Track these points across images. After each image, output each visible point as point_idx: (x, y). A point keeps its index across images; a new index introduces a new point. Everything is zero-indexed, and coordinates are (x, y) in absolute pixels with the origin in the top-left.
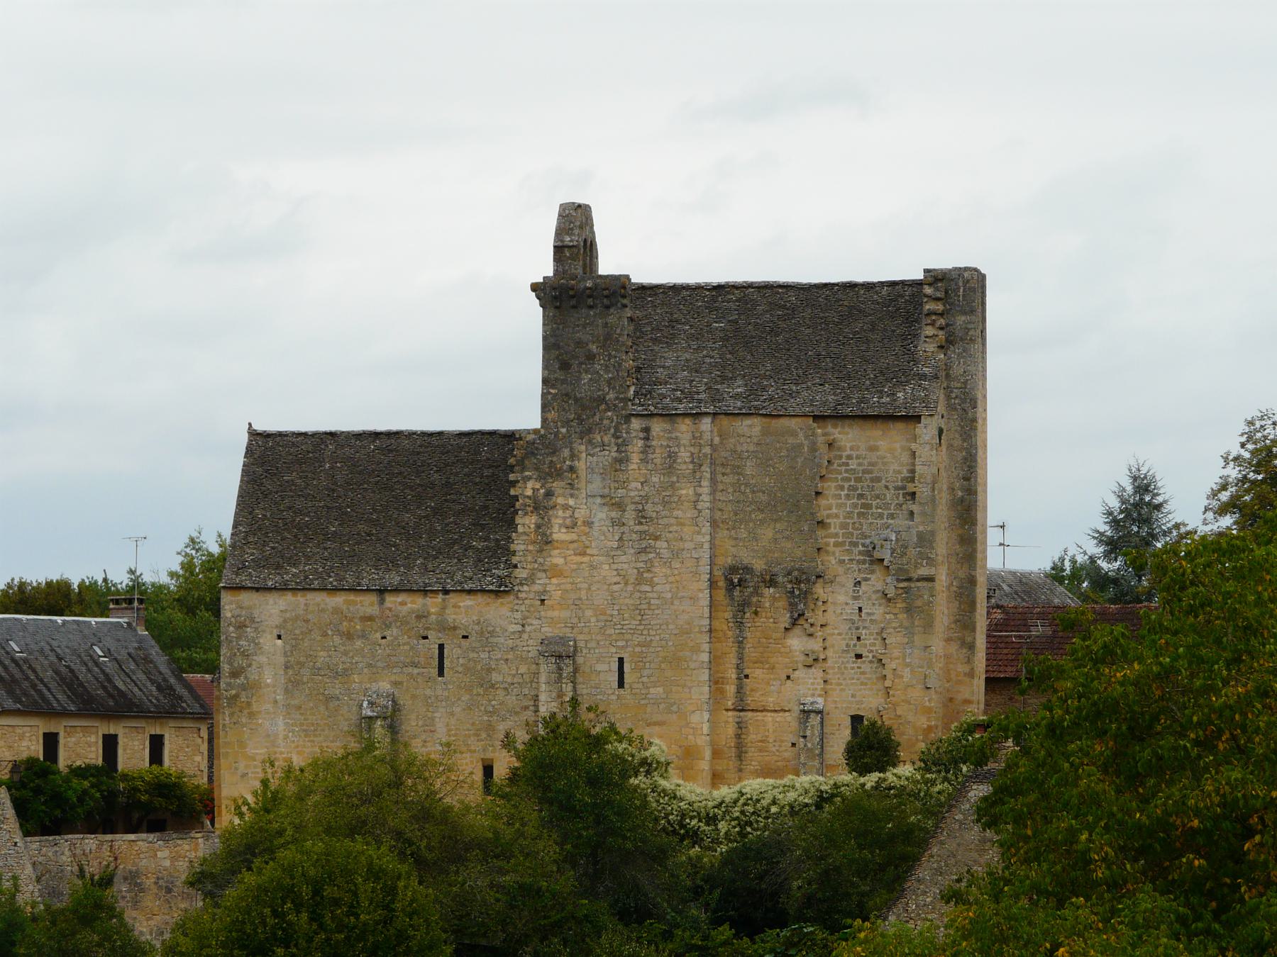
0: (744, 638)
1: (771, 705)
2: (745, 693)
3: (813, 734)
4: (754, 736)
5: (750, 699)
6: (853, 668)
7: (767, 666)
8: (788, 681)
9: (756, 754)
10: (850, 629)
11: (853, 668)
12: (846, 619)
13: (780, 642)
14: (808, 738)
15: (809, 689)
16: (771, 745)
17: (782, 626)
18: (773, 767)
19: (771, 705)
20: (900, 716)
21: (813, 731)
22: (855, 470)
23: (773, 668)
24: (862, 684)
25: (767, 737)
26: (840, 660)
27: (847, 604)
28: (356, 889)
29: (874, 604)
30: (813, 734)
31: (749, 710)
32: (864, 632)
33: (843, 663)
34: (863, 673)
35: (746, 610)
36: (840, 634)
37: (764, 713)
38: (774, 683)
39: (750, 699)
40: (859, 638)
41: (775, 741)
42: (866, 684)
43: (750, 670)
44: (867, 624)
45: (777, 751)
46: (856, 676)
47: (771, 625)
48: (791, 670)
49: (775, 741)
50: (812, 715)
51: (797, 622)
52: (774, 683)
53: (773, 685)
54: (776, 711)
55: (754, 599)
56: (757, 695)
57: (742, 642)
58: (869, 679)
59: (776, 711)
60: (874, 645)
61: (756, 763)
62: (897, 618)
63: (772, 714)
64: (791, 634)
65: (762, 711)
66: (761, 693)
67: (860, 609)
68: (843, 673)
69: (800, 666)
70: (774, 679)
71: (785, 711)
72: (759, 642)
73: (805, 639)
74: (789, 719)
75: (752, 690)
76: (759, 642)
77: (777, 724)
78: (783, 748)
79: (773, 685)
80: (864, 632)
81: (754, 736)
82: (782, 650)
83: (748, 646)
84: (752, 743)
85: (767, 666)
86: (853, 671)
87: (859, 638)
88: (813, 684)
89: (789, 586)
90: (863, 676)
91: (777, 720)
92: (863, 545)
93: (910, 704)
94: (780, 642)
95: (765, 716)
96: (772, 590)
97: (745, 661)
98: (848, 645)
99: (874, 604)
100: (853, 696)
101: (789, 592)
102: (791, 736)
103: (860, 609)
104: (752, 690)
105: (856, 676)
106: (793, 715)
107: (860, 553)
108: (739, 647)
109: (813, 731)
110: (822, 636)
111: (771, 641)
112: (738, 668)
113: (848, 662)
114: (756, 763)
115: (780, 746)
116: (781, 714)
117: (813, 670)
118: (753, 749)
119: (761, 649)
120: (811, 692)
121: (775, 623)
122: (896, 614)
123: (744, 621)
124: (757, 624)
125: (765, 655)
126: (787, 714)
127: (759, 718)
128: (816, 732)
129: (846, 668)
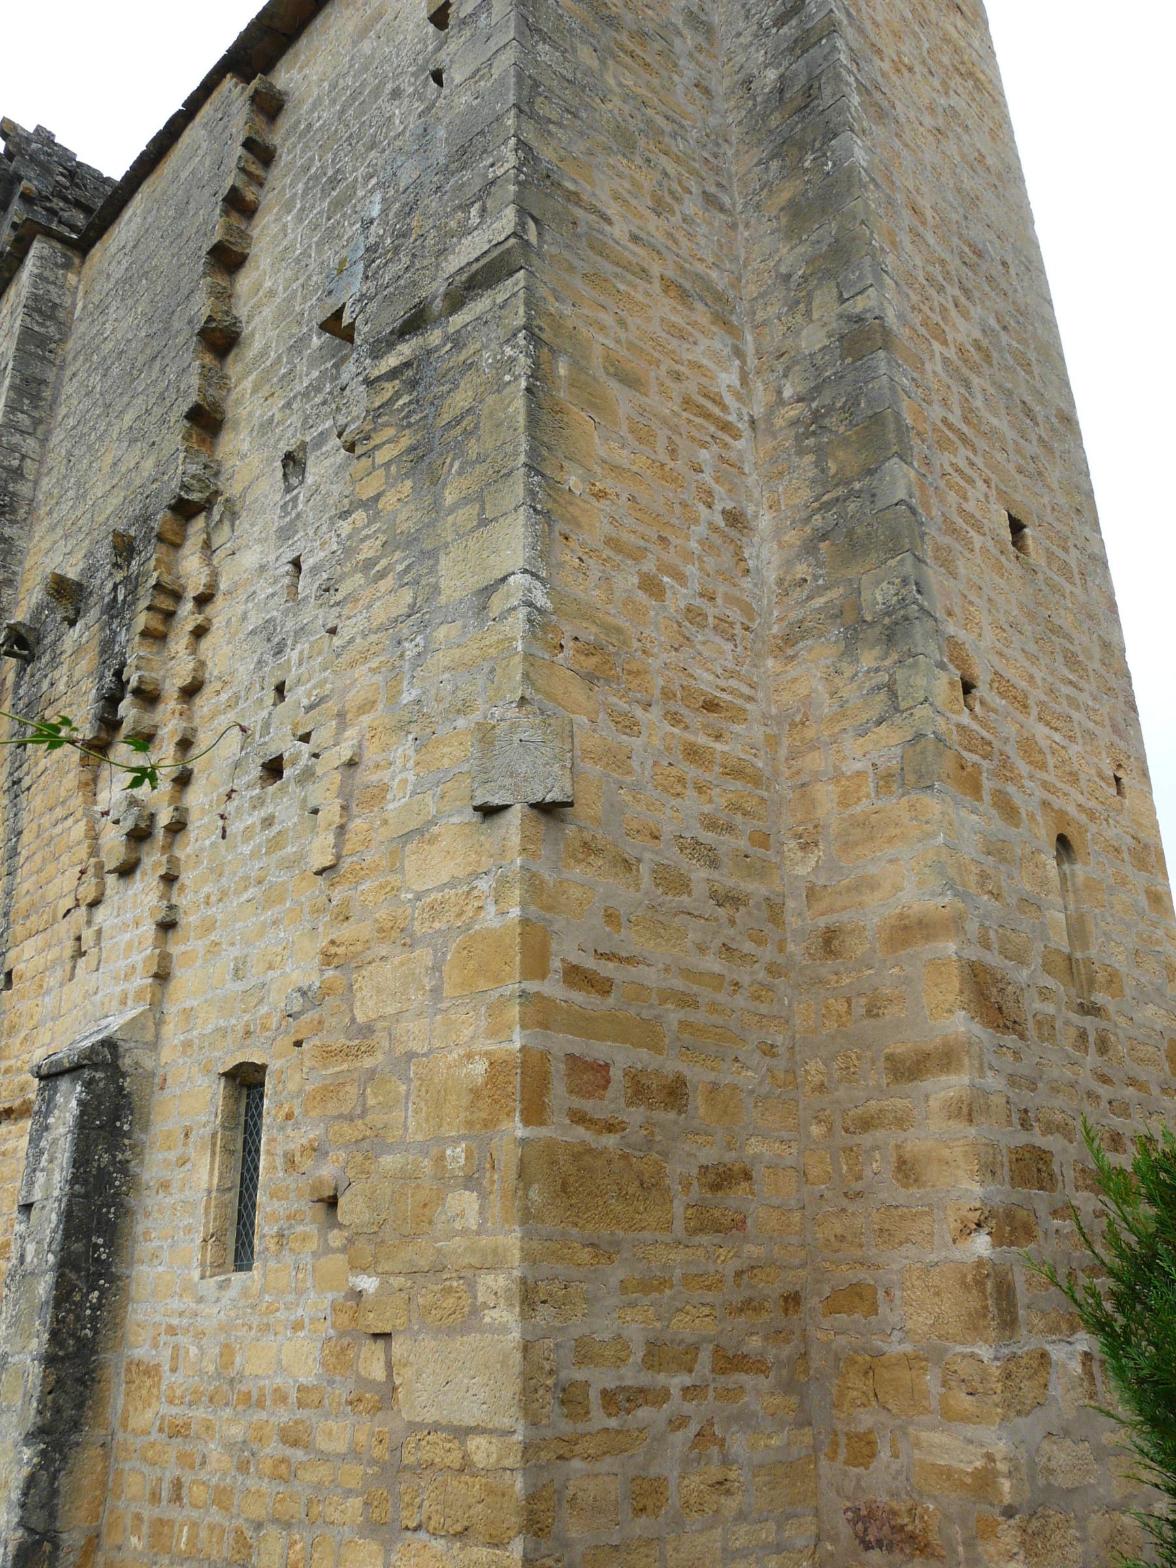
20: (368, 1030)
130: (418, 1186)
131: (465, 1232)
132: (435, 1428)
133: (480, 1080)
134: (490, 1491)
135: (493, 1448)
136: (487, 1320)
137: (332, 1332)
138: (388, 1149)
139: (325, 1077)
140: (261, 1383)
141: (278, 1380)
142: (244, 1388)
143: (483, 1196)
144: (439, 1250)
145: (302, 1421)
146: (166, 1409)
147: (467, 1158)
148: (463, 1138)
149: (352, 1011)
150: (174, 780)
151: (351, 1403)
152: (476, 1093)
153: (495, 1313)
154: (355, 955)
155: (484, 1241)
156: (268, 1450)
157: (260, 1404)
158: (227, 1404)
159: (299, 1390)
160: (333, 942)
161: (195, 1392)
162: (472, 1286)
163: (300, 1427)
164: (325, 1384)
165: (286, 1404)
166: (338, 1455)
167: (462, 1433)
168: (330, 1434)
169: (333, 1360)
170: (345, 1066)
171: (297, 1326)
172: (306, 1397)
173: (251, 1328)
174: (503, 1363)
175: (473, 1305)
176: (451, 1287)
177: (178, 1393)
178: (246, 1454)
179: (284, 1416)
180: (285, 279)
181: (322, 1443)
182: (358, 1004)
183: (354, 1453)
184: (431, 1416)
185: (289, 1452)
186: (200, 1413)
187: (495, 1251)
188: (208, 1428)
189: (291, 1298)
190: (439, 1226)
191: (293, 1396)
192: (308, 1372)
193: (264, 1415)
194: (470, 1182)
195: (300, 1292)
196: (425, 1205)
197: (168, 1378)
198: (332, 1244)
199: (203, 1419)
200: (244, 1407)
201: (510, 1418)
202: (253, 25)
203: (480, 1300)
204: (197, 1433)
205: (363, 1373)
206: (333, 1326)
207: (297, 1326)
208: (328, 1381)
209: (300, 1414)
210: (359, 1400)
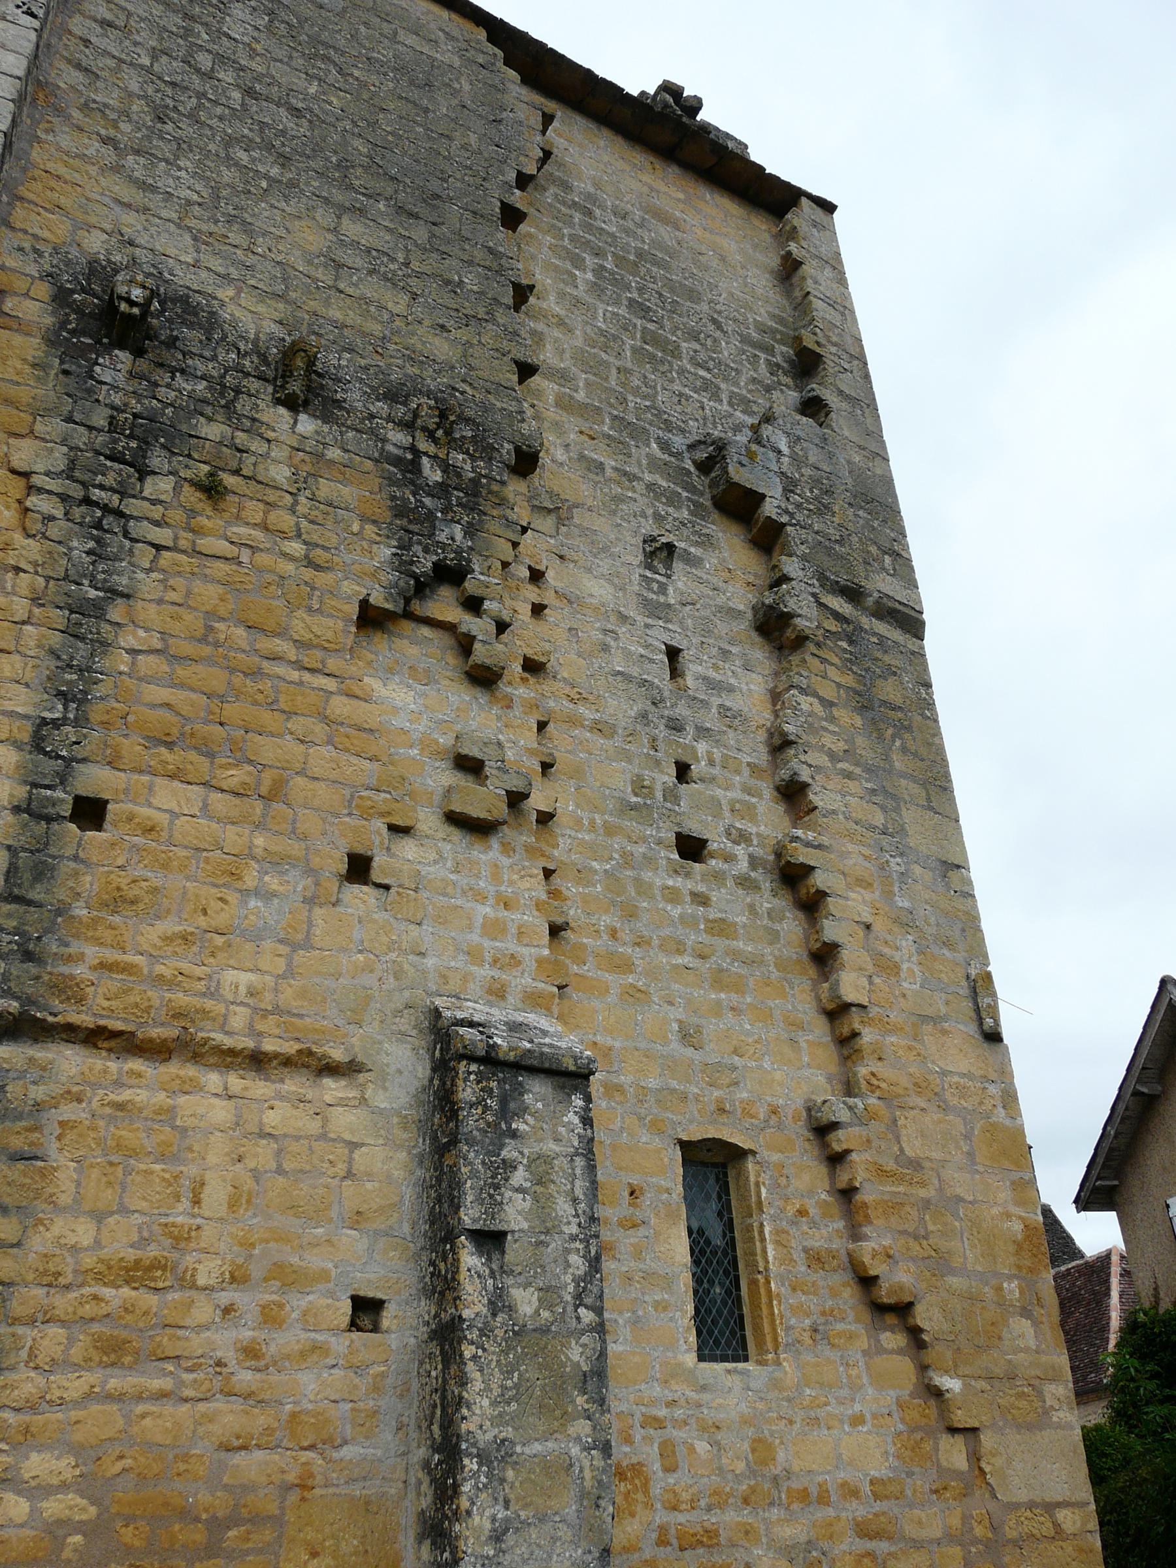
0: (114, 593)
1: (239, 1018)
2: (61, 910)
3: (546, 1228)
4: (83, 1232)
5: (92, 953)
6: (673, 895)
7: (236, 776)
8: (359, 896)
9: (73, 1385)
10: (644, 715)
11: (673, 895)
12: (627, 677)
13: (333, 664)
14: (514, 1251)
15: (475, 956)
16: (203, 1311)
17: (353, 590)
18: (202, 1497)
19: (239, 1018)
20: (916, 1164)
21: (542, 1205)
22: (613, 235)
23: (275, 794)
24: (719, 980)
25: (180, 1239)
26: (617, 843)
27: (623, 618)
28: (681, 1511)
29: (725, 654)
30: (546, 1228)
31: (71, 1033)
32: (702, 747)
33: (627, 860)
34: (720, 928)
35: (157, 459)
36: (599, 728)
37: (174, 1069)
38: (272, 882)
39: (92, 953)
40: (683, 771)
41: (237, 1278)
42: (738, 987)
43: (119, 779)
44: (711, 720)
45: (250, 1352)
46: (692, 938)
47: (289, 568)
48: (380, 825)
49: (237, 1278)
50: (537, 1092)
51: (417, 607)
52: (272, 882)
53: (268, 896)
54: (257, 1061)
55: (213, 431)
56: (152, 934)
57: (97, 610)
58: (751, 962)
59: (257, 1061)
60: (749, 812)
61: (61, 1466)
62: (832, 719)
63: (235, 1082)
64: (381, 647)
65: (158, 1051)
66: (169, 926)
67: (673, 653)
68: (631, 914)
69: (428, 820)
70: (275, 862)
71: (330, 1069)
72: (206, 636)
73: (460, 695)
74: (345, 1121)
75: (117, 901)
76: (206, 636)
77: (263, 1154)
78: (289, 1339)
79: (268, 896)
80: (702, 747)
81: (83, 1232)
82: (340, 706)
83: (128, 640)
84: (51, 1281)
85: (236, 776)
86: (676, 912)
87: (683, 771)
88: (494, 929)
89: (398, 437)
90: (720, 943)
91: (272, 1119)
92: (665, 446)
93: (944, 1108)
94: (333, 664)
95: (190, 1088)
96: (307, 424)
97: (97, 712)
98: (639, 786)
99: (725, 654)
100: (689, 1036)
101: (397, 461)
102: (352, 1241)
103: (673, 653)
104: (117, 901)
105: (692, 938)
106: (381, 1100)
107: (654, 465)
108: (72, 633)
109: (542, 1205)
110: (533, 706)
111: (282, 646)
112: (38, 744)
113: (649, 861)
114: (61, 1466)
115: (271, 1317)
116: (294, 1084)
117: (488, 854)
118: (52, 1339)
119: (217, 679)
120: (485, 972)
121: (310, 563)
122: (832, 704)
123: (132, 506)
124: (208, 544)
125: (231, 710)
126: (333, 1088)
127: (140, 1096)
128: (563, 1207)
129: (643, 888)
130: (983, 1308)
131: (1026, 1350)
132: (1031, 1505)
133: (1020, 1237)
134: (1081, 1550)
135: (1077, 1518)
136: (1055, 1419)
137: (901, 1427)
138: (952, 1271)
139: (883, 1193)
140: (820, 1479)
141: (842, 1475)
142: (795, 1485)
143: (1036, 1324)
144: (1010, 1361)
145: (884, 1513)
146: (661, 1517)
147: (1020, 1293)
148: (1015, 1276)
149: (899, 1142)
150: (707, 841)
151: (936, 1492)
152: (1019, 1246)
153: (1061, 1414)
154: (898, 1096)
155: (1043, 1359)
156: (844, 1547)
157: (823, 1499)
158: (772, 1504)
159: (871, 1482)
160: (873, 1074)
161: (715, 1493)
162: (1040, 1394)
163: (882, 1519)
164: (904, 1476)
165: (857, 1498)
166: (931, 1541)
167: (1050, 1507)
168: (920, 1522)
169: (908, 1453)
170: (901, 1189)
171: (857, 1420)
172: (880, 1489)
173: (791, 1422)
174: (1075, 1452)
175: (1043, 1407)
176: (1023, 1392)
177: (685, 1496)
178: (814, 1554)
179: (859, 1510)
180: (653, 373)
181: (910, 1530)
182: (905, 1139)
183: (950, 1537)
184: (1023, 1496)
185: (870, 1545)
186: (729, 1518)
187: (1053, 1367)
188: (747, 1533)
189: (844, 1392)
190: (1007, 1343)
191: (867, 1489)
192: (879, 1468)
193: (831, 1512)
194: (1025, 1313)
195: (855, 1387)
196: (993, 1324)
197: (660, 1482)
198: (885, 1346)
199: (738, 1524)
200: (801, 1506)
201: (1085, 1492)
202: (541, 46)
203: (1048, 1403)
204: (730, 1540)
205: (945, 1464)
206: (903, 1420)
207: (857, 1420)
208: (907, 1473)
209: (878, 1506)
210: (945, 1488)
